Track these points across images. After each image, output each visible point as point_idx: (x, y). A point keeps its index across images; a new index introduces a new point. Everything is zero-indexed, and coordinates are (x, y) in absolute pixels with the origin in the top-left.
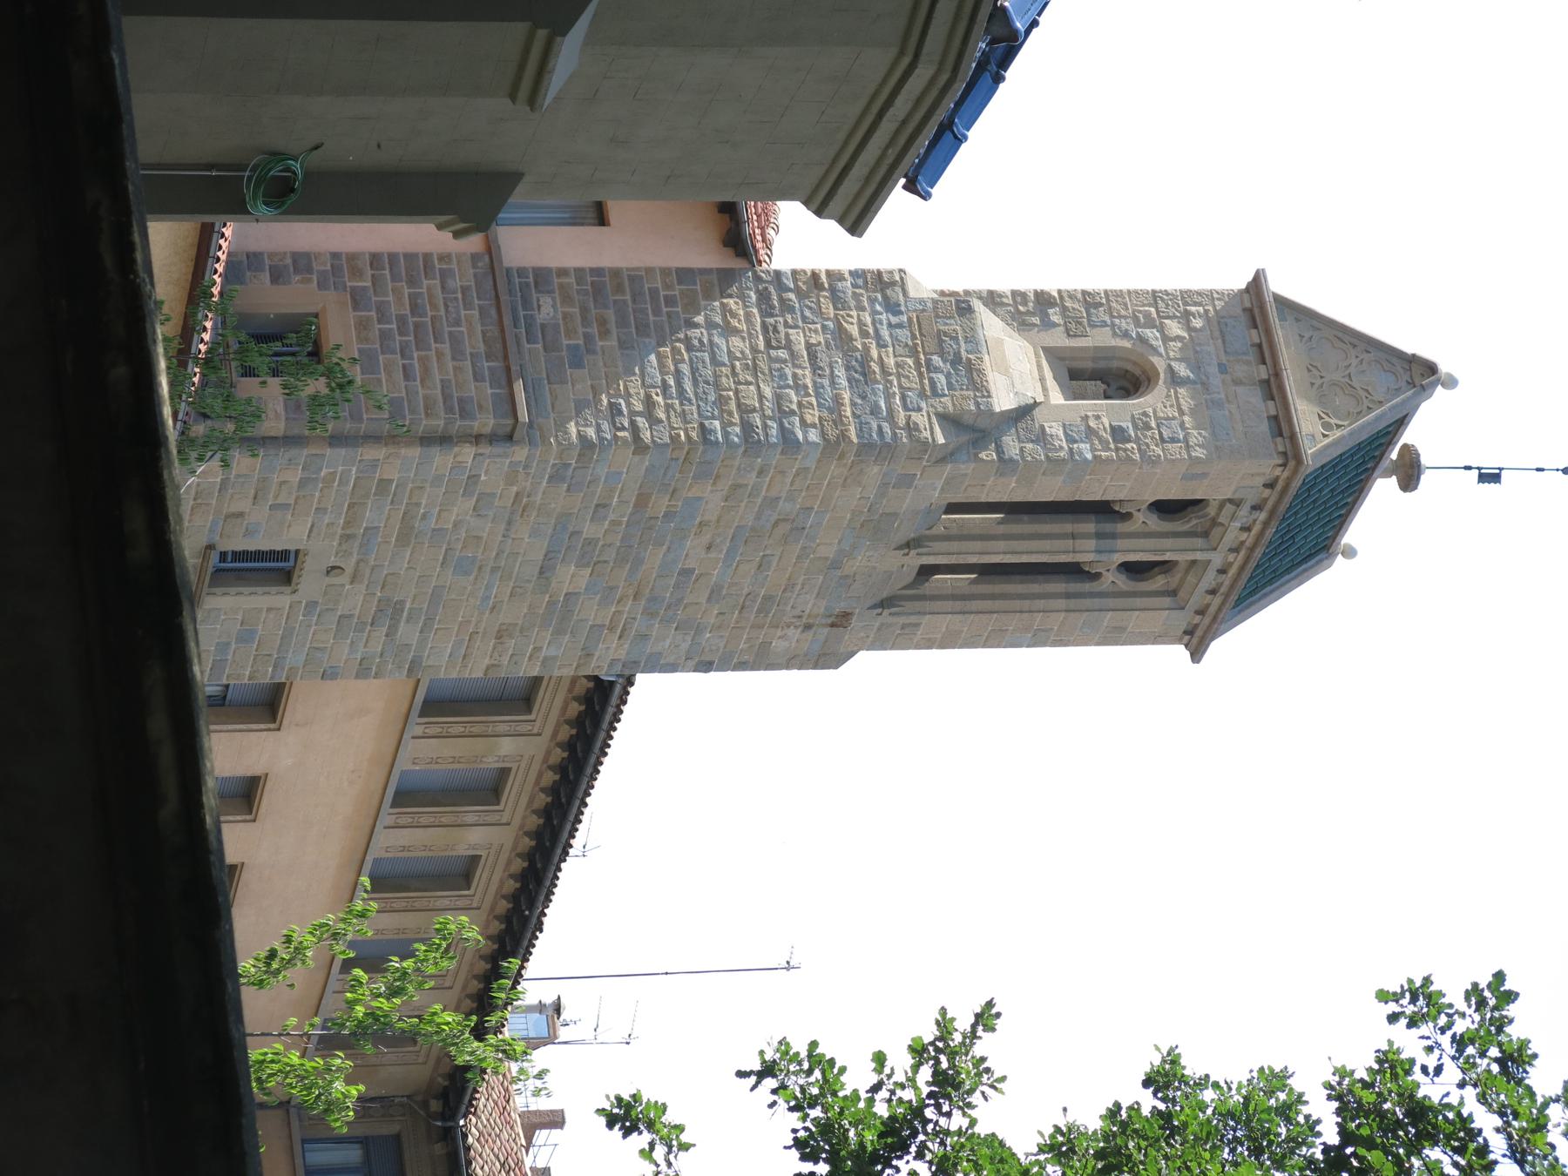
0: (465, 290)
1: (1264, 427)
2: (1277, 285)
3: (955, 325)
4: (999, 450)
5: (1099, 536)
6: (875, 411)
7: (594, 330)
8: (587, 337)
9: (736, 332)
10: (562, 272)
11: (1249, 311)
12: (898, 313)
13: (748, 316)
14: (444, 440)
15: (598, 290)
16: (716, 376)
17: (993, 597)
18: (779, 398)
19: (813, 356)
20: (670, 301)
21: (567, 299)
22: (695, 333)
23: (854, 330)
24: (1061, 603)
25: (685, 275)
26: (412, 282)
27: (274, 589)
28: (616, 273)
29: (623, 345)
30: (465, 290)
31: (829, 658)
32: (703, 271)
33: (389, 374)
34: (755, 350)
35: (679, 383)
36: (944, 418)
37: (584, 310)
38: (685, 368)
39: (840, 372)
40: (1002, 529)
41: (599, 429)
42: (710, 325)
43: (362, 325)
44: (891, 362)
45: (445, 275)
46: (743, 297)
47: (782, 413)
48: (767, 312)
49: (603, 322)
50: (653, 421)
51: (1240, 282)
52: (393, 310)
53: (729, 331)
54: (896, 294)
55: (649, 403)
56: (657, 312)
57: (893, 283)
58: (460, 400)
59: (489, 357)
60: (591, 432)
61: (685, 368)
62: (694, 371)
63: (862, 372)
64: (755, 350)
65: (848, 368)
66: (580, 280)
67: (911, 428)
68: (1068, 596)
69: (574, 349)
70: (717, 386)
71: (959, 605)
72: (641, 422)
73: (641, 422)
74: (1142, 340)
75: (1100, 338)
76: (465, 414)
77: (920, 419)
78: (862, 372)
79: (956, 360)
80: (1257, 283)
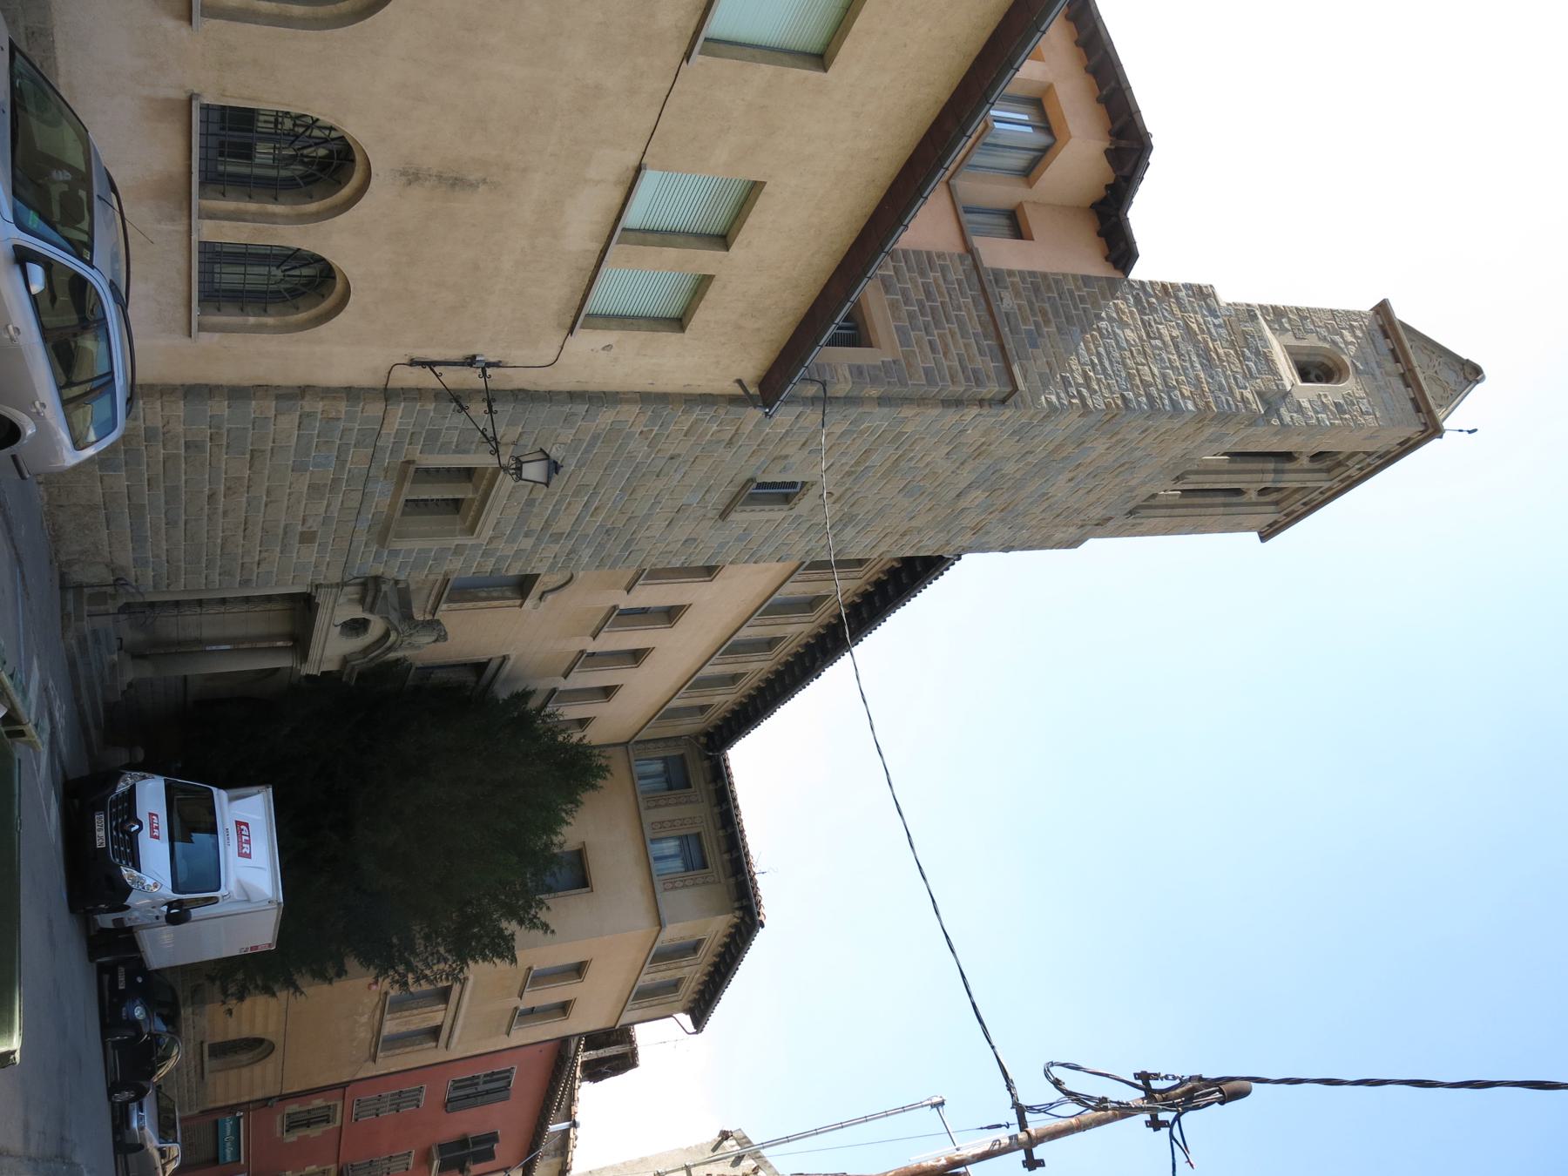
0: (959, 282)
1: (1410, 405)
2: (1401, 313)
3: (1249, 328)
4: (1281, 420)
5: (1276, 471)
6: (1221, 388)
7: (1040, 319)
8: (1036, 324)
9: (1128, 325)
10: (1011, 273)
11: (1382, 327)
12: (1217, 317)
13: (1131, 313)
14: (957, 403)
15: (1036, 290)
16: (1123, 358)
17: (1193, 506)
18: (1164, 376)
19: (1176, 347)
20: (1082, 299)
21: (1017, 295)
22: (1103, 324)
23: (1195, 326)
24: (1221, 510)
25: (1087, 280)
26: (923, 274)
27: (776, 507)
28: (1044, 276)
29: (1059, 330)
30: (959, 282)
31: (1073, 543)
32: (1098, 279)
33: (921, 348)
34: (1140, 338)
35: (1101, 363)
36: (1260, 394)
37: (1030, 303)
38: (1102, 350)
39: (1194, 358)
40: (1227, 466)
41: (1059, 398)
42: (1110, 319)
43: (894, 306)
44: (1221, 351)
45: (943, 269)
46: (1126, 300)
47: (1169, 389)
48: (1142, 312)
49: (1044, 313)
50: (1093, 392)
51: (1366, 304)
52: (913, 296)
53: (1123, 325)
54: (1211, 301)
55: (1085, 375)
56: (1076, 308)
57: (1209, 295)
58: (974, 371)
59: (986, 337)
60: (1054, 398)
61: (1102, 350)
62: (1108, 353)
63: (1206, 356)
64: (1140, 338)
65: (1198, 356)
66: (1023, 281)
67: (1244, 400)
68: (1225, 505)
69: (1029, 332)
70: (1125, 365)
71: (1169, 511)
72: (1084, 391)
73: (1084, 391)
74: (1334, 343)
75: (1312, 341)
76: (978, 382)
77: (1248, 394)
78: (1206, 356)
79: (1257, 353)
80: (1383, 309)
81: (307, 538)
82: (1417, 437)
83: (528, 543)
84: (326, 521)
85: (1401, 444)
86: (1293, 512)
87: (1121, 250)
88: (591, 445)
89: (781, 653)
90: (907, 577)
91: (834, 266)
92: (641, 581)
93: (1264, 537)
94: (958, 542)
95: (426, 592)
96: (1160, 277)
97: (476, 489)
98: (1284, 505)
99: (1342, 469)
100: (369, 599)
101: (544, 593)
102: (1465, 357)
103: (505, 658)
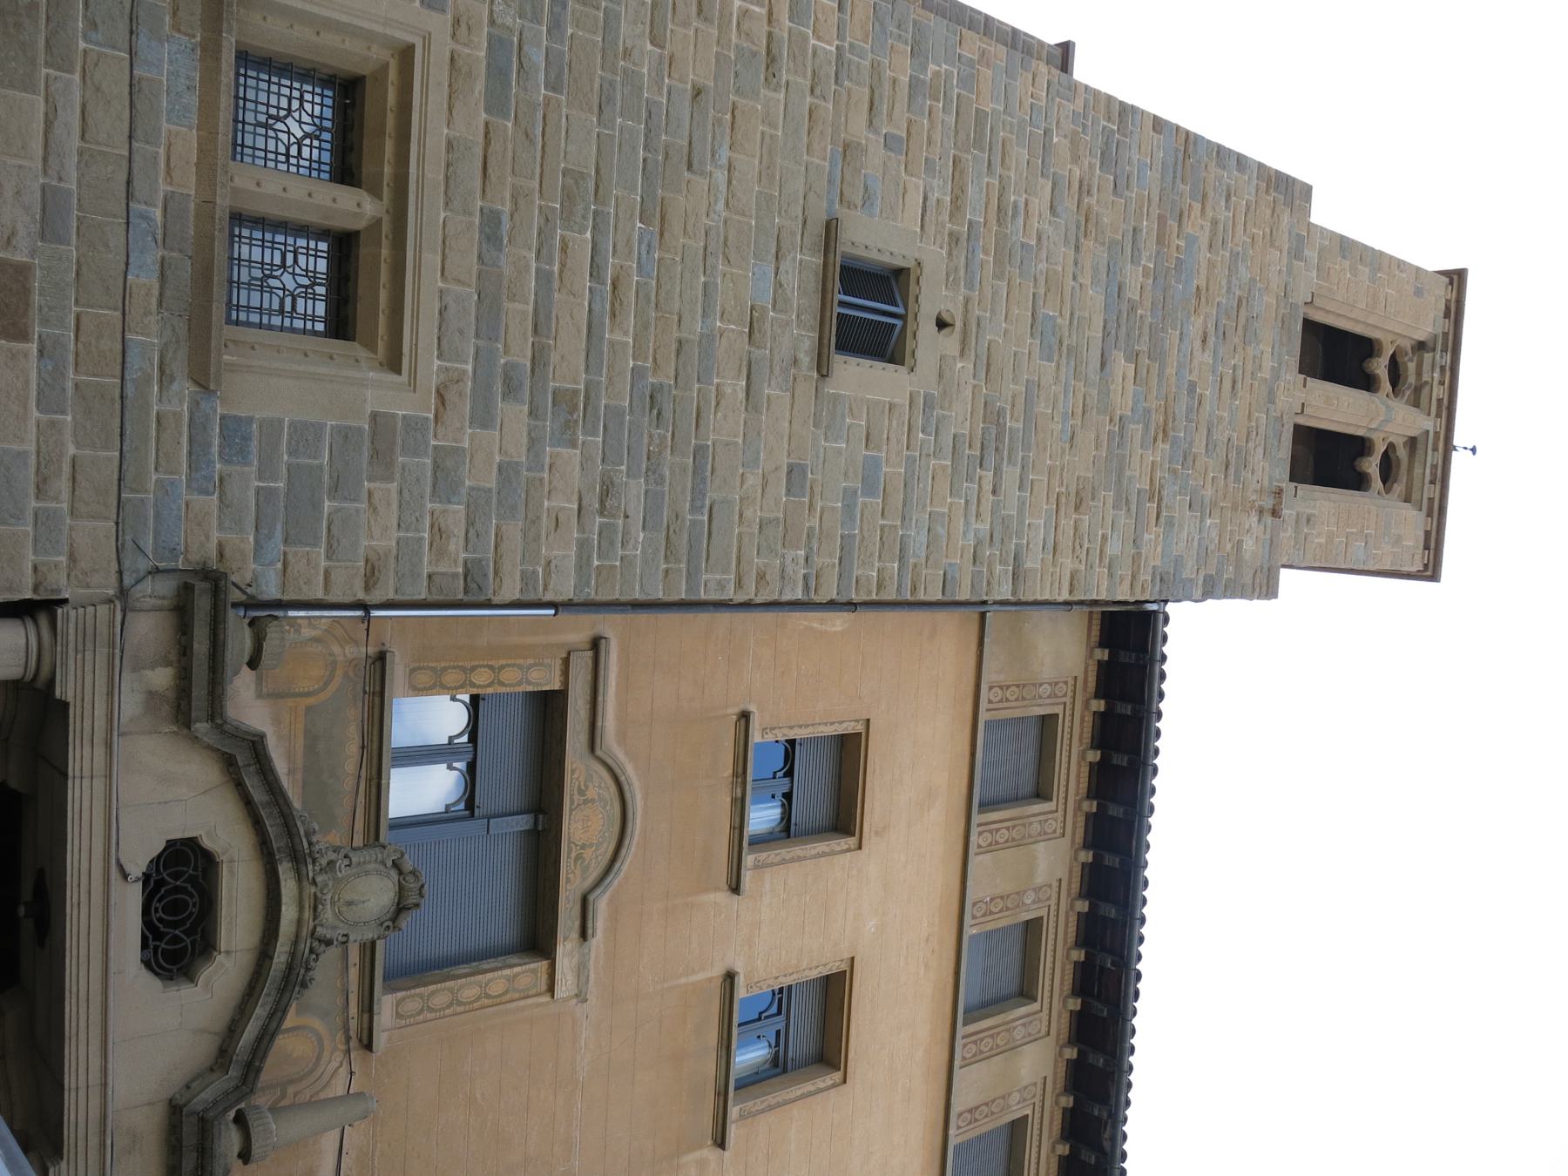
90: (1127, 651)
92: (734, 1111)
97: (376, 193)
99: (1425, 391)
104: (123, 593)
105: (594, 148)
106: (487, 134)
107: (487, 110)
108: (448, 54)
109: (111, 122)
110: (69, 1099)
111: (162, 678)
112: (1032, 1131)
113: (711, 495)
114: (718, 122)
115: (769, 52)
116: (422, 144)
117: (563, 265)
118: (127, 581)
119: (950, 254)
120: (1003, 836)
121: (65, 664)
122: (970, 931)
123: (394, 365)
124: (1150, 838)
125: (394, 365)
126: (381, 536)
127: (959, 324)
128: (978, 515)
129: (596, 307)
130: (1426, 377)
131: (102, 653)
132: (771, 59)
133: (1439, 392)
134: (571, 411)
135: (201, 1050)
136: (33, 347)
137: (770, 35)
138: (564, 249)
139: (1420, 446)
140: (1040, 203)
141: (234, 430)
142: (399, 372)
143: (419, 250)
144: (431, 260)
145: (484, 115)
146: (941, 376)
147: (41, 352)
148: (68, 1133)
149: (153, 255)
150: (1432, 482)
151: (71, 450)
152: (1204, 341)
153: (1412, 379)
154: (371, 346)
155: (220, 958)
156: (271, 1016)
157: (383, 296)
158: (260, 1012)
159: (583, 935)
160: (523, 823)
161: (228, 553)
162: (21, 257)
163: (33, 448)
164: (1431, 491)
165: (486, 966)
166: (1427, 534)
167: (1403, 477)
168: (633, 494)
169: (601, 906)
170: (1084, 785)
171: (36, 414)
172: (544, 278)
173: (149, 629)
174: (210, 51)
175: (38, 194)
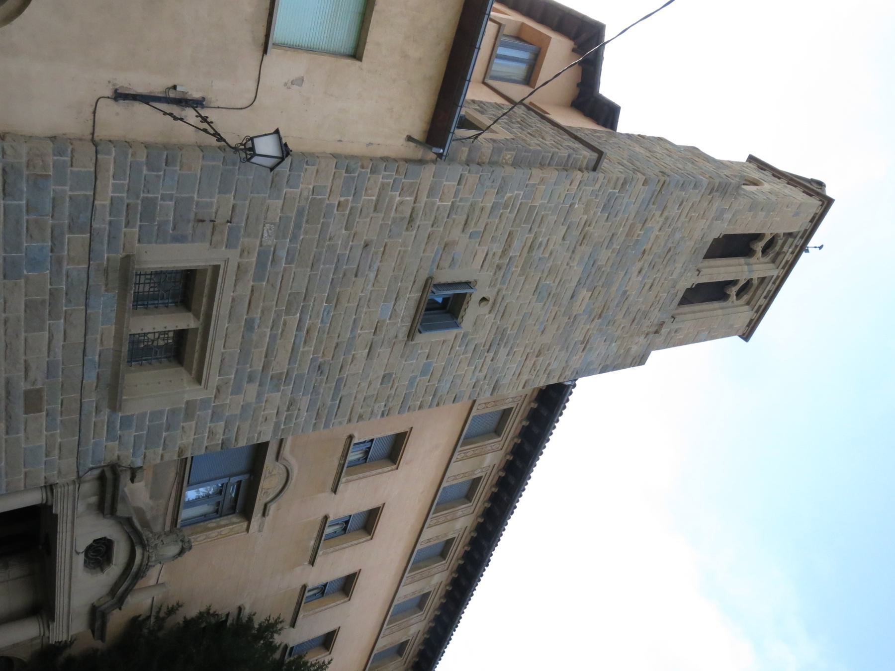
81: (33, 401)
82: (819, 211)
83: (251, 390)
84: (50, 371)
85: (811, 221)
86: (760, 306)
87: (607, 114)
88: (298, 226)
89: (433, 603)
90: (549, 402)
91: (455, 31)
92: (343, 480)
93: (746, 336)
94: (576, 362)
95: (161, 520)
96: (635, 131)
97: (197, 316)
98: (753, 303)
99: (781, 256)
100: (107, 504)
101: (266, 505)
102: (810, 178)
103: (240, 609)
104: (79, 477)
105: (307, 281)
106: (252, 291)
107: (253, 281)
108: (236, 265)
109: (77, 335)
110: (58, 560)
111: (94, 499)
112: (482, 484)
113: (342, 393)
114: (376, 253)
115: (411, 216)
116: (220, 302)
117: (283, 330)
118: (81, 473)
119: (495, 273)
120: (471, 453)
121: (57, 500)
122: (473, 413)
123: (199, 379)
124: (537, 463)
125: (199, 379)
126: (187, 439)
127: (491, 301)
128: (480, 371)
129: (297, 342)
130: (785, 249)
131: (71, 500)
132: (412, 219)
133: (789, 257)
134: (278, 381)
135: (105, 590)
136: (44, 413)
137: (413, 209)
138: (285, 324)
139: (766, 281)
140: (557, 237)
141: (126, 422)
142: (200, 383)
143: (214, 340)
144: (219, 344)
145: (252, 283)
146: (475, 324)
147: (47, 415)
148: (57, 611)
149: (94, 375)
150: (765, 298)
151: (59, 440)
152: (640, 272)
153: (777, 248)
154: (189, 371)
155: (113, 566)
156: (130, 585)
157: (196, 355)
158: (126, 584)
159: (264, 515)
160: (244, 478)
161: (122, 458)
162: (38, 386)
163: (44, 443)
164: (762, 302)
165: (223, 523)
166: (751, 320)
167: (751, 293)
168: (304, 402)
169: (273, 507)
170: (518, 431)
171: (45, 432)
172: (273, 338)
173: (89, 487)
174: (122, 297)
175: (46, 366)
